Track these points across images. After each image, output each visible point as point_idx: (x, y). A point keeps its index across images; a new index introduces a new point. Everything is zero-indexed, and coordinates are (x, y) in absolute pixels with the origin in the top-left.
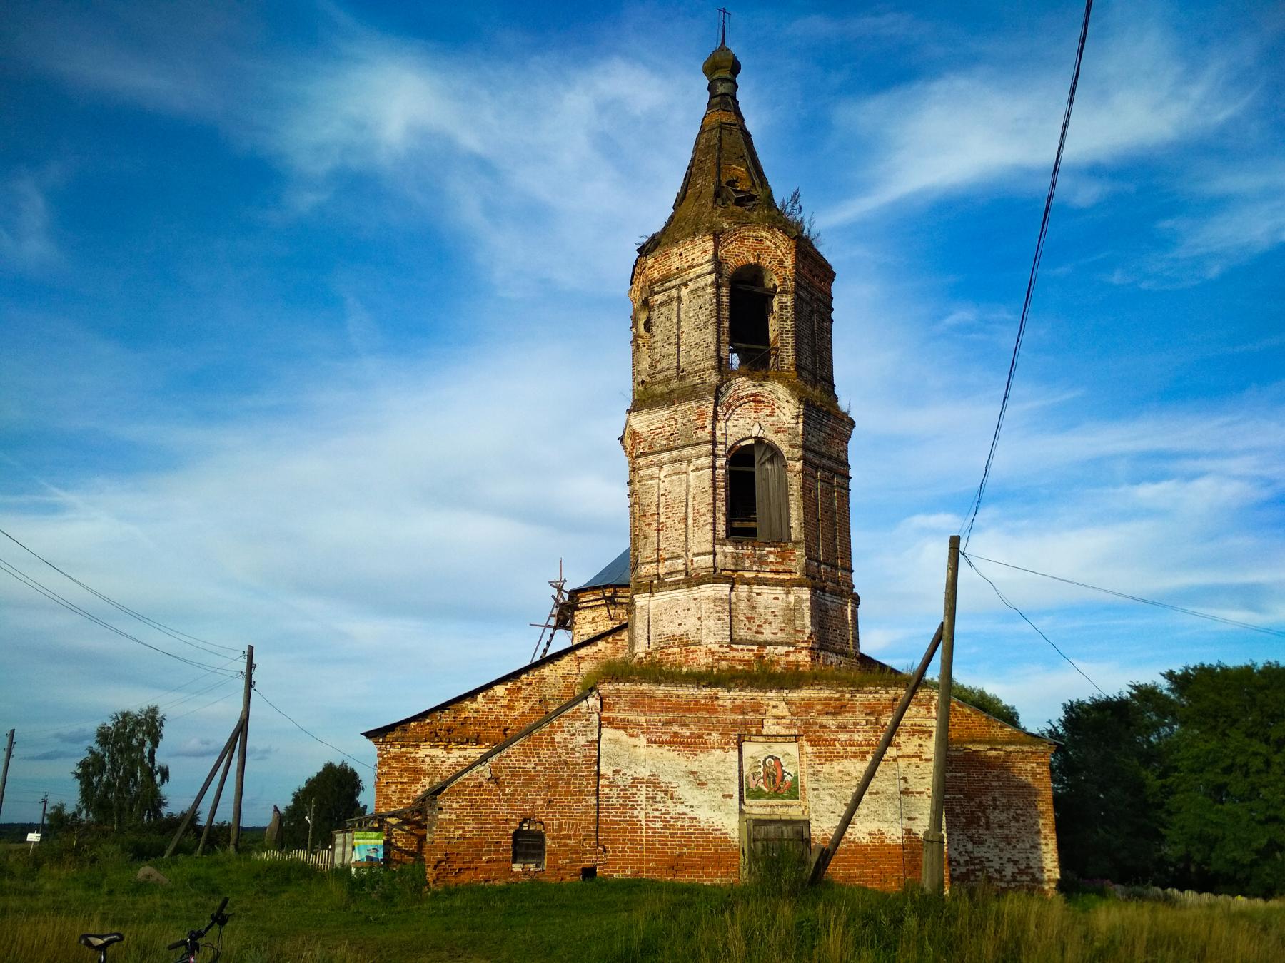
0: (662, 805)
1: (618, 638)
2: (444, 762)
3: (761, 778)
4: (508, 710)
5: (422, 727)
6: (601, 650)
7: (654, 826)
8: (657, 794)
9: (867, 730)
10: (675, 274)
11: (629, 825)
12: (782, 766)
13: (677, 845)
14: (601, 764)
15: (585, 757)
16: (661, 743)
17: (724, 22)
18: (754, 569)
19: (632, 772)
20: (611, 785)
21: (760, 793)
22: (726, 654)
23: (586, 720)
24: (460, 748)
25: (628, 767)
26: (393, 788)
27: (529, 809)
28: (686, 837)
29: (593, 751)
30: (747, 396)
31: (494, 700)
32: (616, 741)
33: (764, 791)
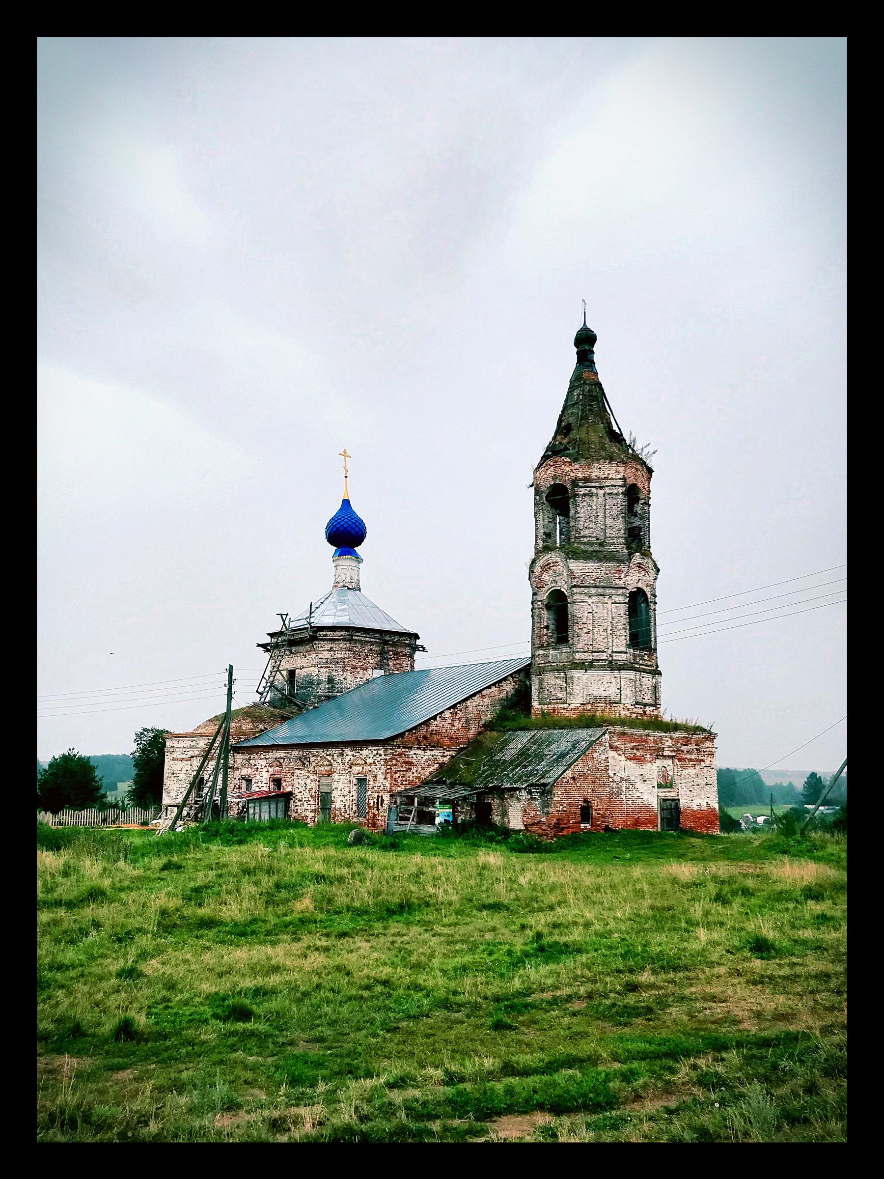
16: (630, 759)
26: (398, 775)
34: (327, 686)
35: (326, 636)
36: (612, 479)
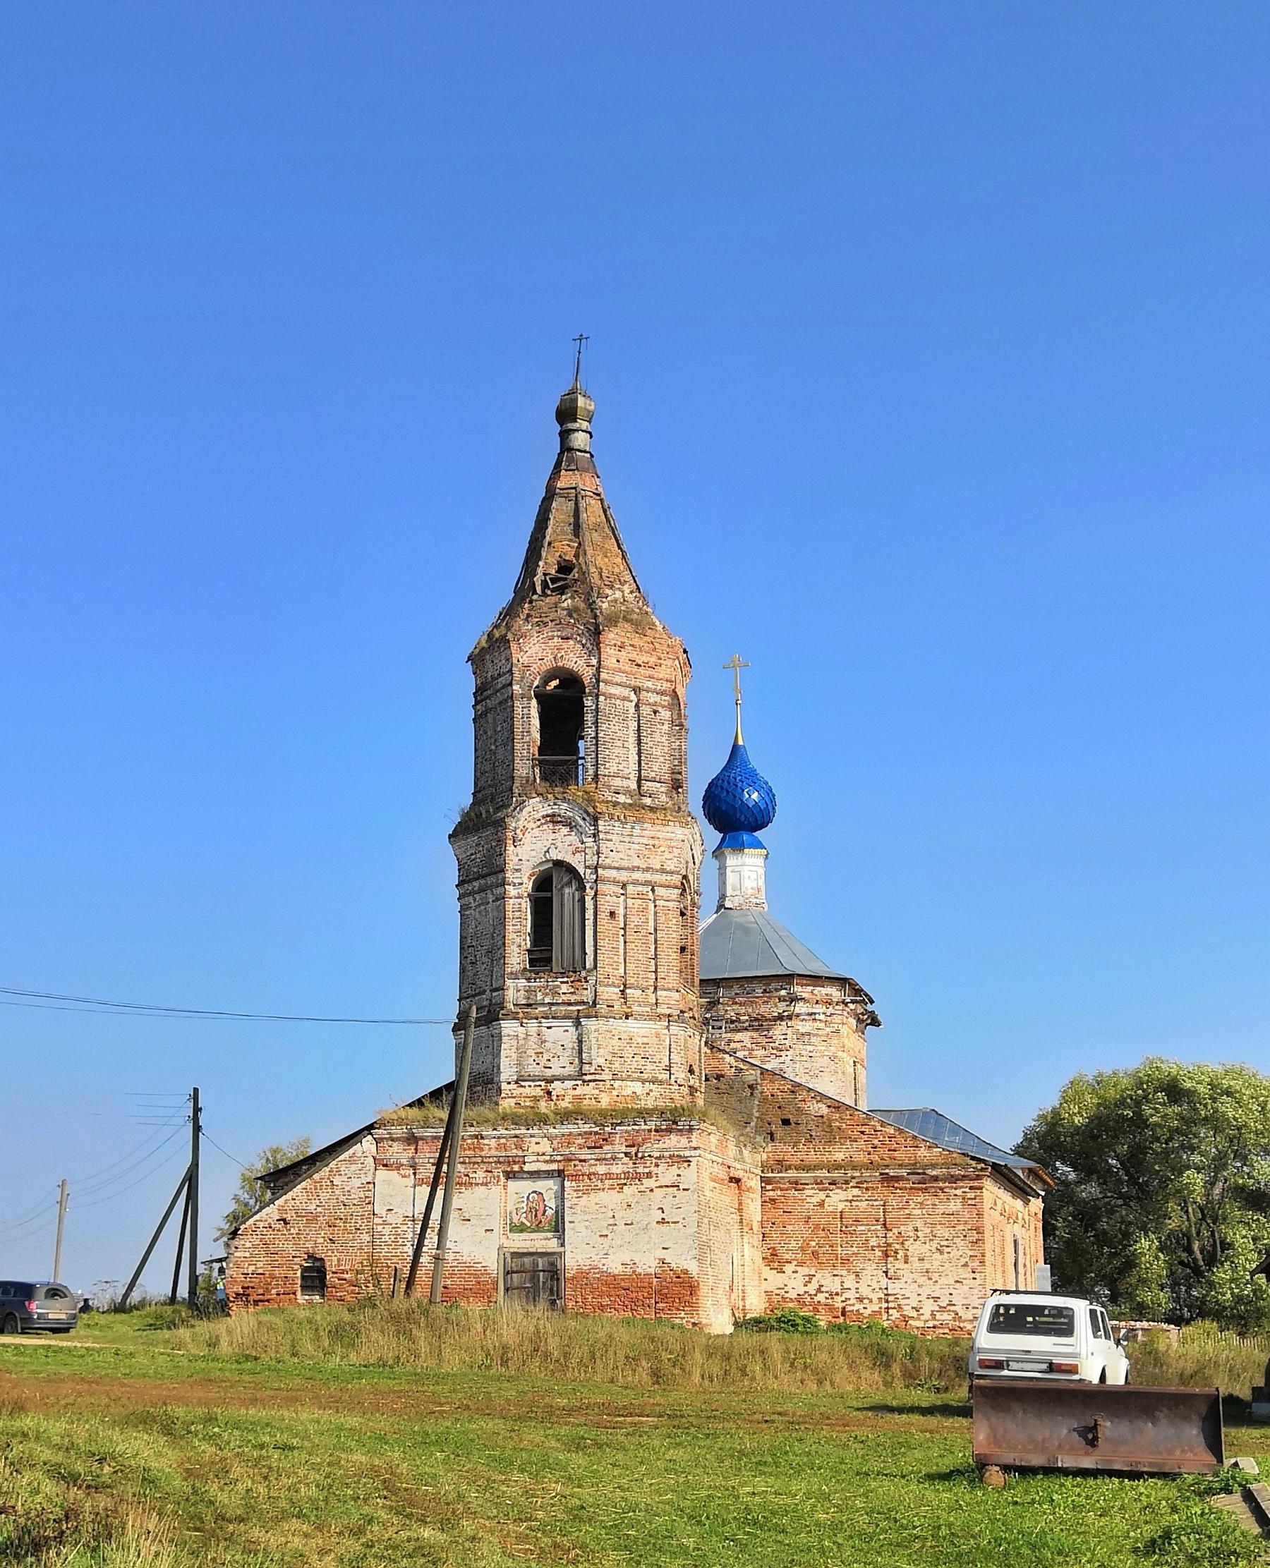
12: (544, 1200)
17: (579, 353)
18: (546, 1002)
20: (385, 1223)
22: (513, 1091)
23: (362, 1164)
25: (399, 1207)
32: (389, 1183)
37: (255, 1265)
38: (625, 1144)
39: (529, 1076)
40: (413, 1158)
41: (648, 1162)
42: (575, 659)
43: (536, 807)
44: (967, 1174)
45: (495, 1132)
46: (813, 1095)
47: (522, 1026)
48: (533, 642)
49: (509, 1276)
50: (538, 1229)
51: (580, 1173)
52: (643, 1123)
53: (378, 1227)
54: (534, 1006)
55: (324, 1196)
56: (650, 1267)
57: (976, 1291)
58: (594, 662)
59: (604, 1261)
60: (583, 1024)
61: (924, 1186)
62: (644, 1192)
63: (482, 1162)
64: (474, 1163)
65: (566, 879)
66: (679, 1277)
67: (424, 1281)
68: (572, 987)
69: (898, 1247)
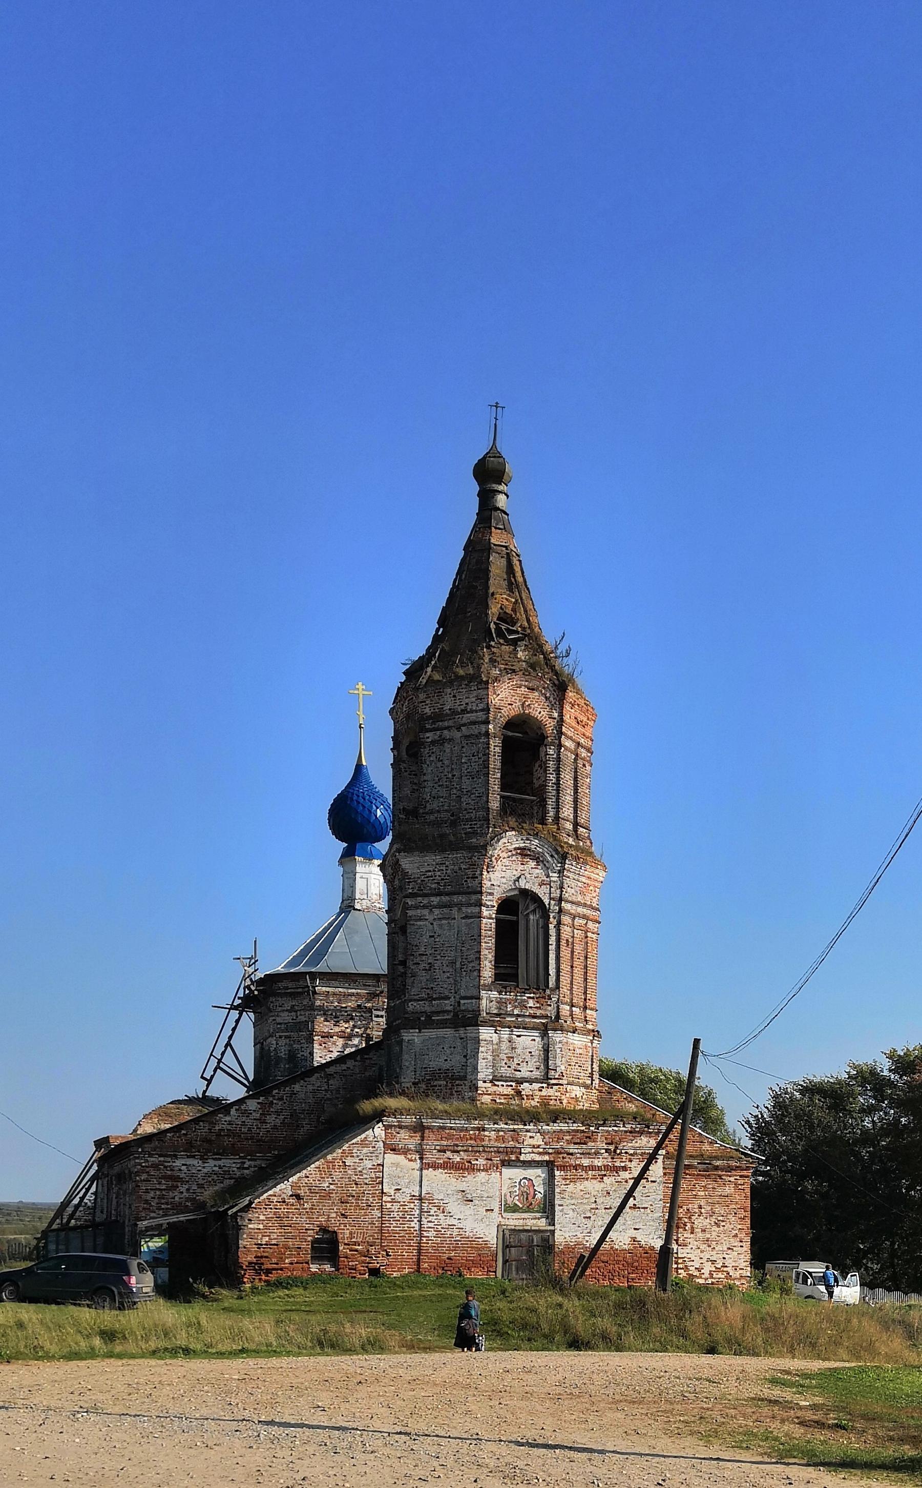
0: (435, 1217)
1: (366, 1056)
2: (200, 1170)
3: (517, 1196)
4: (260, 1123)
5: (178, 1137)
6: (349, 1068)
7: (428, 1235)
8: (430, 1209)
9: (606, 1157)
10: (447, 715)
11: (407, 1234)
13: (446, 1250)
14: (384, 1184)
15: (371, 1178)
17: (496, 419)
18: (515, 1013)
19: (410, 1191)
20: (393, 1201)
21: (515, 1207)
24: (216, 1158)
26: (152, 1194)
27: (324, 1221)
28: (453, 1244)
29: (378, 1173)
30: (515, 849)
31: (247, 1113)
32: (397, 1165)
33: (519, 1206)
34: (287, 1066)
35: (287, 988)
36: (472, 711)
37: (269, 1236)
38: (605, 1141)
39: (502, 1076)
40: (420, 1144)
41: (624, 1158)
42: (540, 710)
43: (511, 840)
44: (741, 1165)
45: (496, 1126)
46: (625, 1097)
47: (496, 1033)
48: (504, 687)
49: (508, 1249)
50: (529, 1209)
51: (568, 1165)
52: (622, 1125)
53: (387, 1204)
54: (502, 1016)
55: (337, 1175)
56: (625, 1244)
57: (742, 1256)
58: (556, 715)
59: (587, 1238)
60: (550, 1035)
61: (708, 1173)
62: (620, 1182)
63: (484, 1151)
64: (477, 1151)
65: (532, 908)
66: (647, 1253)
67: (431, 1253)
68: (538, 1002)
69: (686, 1220)
